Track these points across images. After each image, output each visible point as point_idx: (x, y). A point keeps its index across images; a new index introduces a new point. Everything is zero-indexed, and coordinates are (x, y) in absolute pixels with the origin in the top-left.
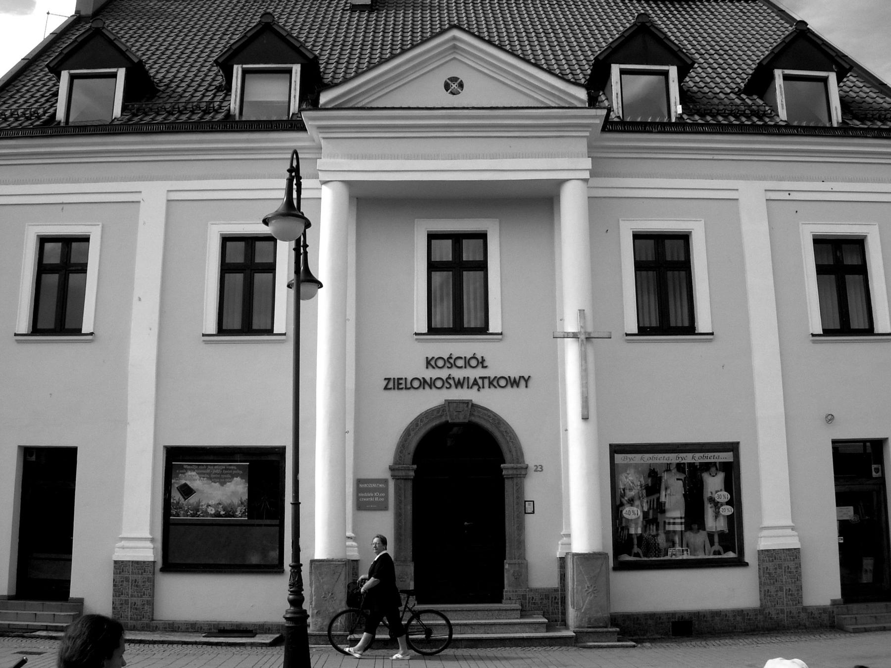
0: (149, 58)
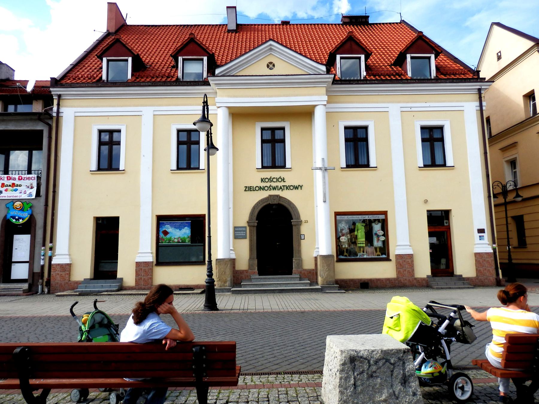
0: (142, 53)
